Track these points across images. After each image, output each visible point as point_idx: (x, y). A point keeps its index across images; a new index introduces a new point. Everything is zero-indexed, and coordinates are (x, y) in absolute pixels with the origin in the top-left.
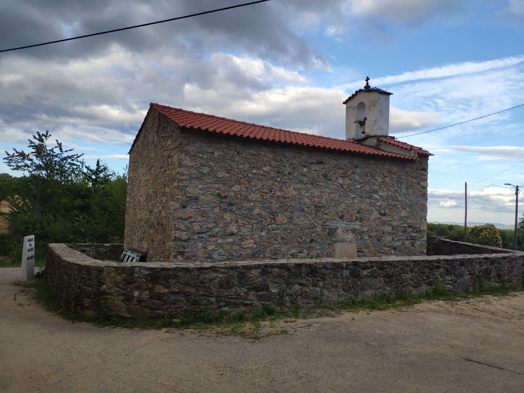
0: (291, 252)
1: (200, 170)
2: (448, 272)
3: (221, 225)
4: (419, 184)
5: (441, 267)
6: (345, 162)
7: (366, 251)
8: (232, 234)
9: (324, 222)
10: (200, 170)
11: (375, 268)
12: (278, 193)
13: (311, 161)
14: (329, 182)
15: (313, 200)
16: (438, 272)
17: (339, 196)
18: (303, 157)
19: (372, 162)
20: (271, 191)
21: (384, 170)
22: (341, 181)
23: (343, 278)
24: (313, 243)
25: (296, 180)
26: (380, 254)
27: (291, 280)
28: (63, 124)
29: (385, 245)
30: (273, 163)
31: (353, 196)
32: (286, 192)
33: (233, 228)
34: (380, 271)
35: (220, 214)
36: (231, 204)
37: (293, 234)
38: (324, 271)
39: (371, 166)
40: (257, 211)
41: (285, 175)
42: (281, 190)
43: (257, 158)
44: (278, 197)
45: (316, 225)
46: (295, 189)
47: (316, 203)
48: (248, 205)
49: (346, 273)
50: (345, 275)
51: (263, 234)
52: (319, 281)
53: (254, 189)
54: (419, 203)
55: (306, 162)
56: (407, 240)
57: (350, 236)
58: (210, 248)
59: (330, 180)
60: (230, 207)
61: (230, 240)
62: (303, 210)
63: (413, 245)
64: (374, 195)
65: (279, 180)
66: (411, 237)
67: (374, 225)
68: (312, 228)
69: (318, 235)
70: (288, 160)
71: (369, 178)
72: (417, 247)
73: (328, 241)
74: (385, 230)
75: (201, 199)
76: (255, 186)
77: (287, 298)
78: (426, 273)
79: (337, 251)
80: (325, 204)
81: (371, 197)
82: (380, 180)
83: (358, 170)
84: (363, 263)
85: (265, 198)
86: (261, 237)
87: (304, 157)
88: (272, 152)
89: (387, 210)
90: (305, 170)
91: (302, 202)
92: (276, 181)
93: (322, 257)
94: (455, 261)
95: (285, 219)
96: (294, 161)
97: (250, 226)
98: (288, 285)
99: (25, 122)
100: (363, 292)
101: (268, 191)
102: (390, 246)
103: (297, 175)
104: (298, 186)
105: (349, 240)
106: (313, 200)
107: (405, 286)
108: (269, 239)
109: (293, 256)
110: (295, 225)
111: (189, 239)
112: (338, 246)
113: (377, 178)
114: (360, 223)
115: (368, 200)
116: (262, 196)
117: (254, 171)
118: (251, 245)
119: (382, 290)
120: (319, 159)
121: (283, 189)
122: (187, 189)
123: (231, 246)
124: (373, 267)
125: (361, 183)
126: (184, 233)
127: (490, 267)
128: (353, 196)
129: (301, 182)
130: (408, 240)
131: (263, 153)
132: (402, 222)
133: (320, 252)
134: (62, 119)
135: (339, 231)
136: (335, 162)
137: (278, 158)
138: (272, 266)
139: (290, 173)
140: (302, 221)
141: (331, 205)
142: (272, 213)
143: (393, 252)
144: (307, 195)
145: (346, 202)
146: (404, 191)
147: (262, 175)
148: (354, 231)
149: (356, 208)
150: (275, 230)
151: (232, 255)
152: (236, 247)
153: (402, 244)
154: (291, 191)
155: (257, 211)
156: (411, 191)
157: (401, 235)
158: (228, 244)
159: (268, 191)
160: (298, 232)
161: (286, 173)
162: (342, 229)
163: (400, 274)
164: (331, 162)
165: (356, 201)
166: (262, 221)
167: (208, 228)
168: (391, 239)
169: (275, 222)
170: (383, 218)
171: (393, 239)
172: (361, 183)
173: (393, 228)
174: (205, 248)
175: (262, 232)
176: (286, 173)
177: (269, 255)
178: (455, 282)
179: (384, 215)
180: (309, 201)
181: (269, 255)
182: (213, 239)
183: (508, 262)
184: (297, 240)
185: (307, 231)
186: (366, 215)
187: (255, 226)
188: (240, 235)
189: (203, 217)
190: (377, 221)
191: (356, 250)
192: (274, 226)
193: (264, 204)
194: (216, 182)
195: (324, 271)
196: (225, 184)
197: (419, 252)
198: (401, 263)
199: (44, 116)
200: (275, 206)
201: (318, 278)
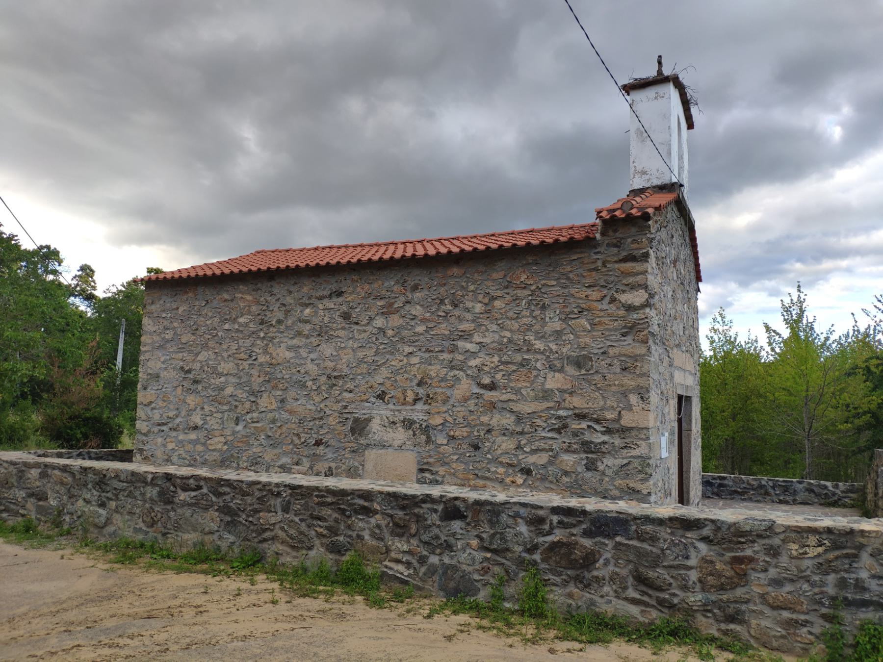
0: (280, 463)
1: (163, 336)
2: (400, 529)
3: (183, 413)
4: (613, 300)
5: (376, 512)
6: (389, 283)
7: (442, 470)
8: (196, 428)
9: (346, 407)
10: (163, 336)
11: (205, 490)
12: (262, 359)
13: (320, 293)
14: (356, 327)
15: (322, 366)
16: (368, 522)
17: (377, 353)
18: (305, 288)
19: (455, 271)
20: (250, 356)
21: (490, 283)
22: (379, 322)
23: (145, 501)
24: (322, 447)
25: (290, 332)
26: (481, 482)
27: (74, 492)
28: (829, 271)
29: (495, 461)
30: (254, 308)
31: (408, 349)
32: (274, 355)
33: (197, 419)
34: (214, 499)
35: (182, 397)
36: (196, 382)
37: (284, 429)
38: (116, 484)
39: (452, 282)
40: (229, 390)
41: (271, 325)
42: (266, 352)
43: (231, 305)
44: (261, 365)
45: (328, 412)
46: (289, 348)
47: (329, 372)
48: (218, 381)
49: (152, 492)
50: (149, 495)
51: (239, 428)
52: (110, 499)
53: (225, 355)
54: (611, 352)
55: (309, 298)
56: (567, 451)
57: (400, 435)
58: (171, 446)
59: (357, 324)
60: (195, 387)
61: (193, 436)
62: (304, 386)
63: (591, 466)
64: (461, 344)
65: (262, 335)
66: (585, 444)
67: (461, 412)
68: (321, 419)
69: (331, 431)
70: (278, 300)
71: (449, 307)
72: (609, 472)
73: (351, 445)
74: (494, 422)
75: (162, 376)
76: (227, 351)
77: (67, 518)
78: (325, 520)
79: (369, 466)
80: (346, 370)
81: (453, 350)
82: (479, 308)
83: (418, 295)
84: (178, 477)
85: (241, 368)
86: (234, 433)
87: (305, 289)
88: (254, 290)
89: (499, 376)
90: (307, 311)
91: (303, 371)
92: (259, 337)
93: (337, 475)
94: (424, 501)
95: (274, 402)
96: (289, 300)
97: (220, 415)
98: (70, 498)
99: (770, 280)
100: (180, 534)
101: (246, 357)
102: (510, 465)
103: (293, 323)
104: (295, 342)
105: (397, 443)
106: (322, 366)
107: (265, 540)
108: (247, 437)
109: (284, 469)
110: (291, 412)
111: (149, 431)
112: (372, 455)
113: (469, 305)
114: (426, 407)
115: (446, 356)
116: (237, 365)
117: (227, 326)
118: (219, 446)
119: (215, 537)
120: (334, 287)
121: (270, 350)
122: (149, 364)
123: (195, 446)
124: (199, 488)
125: (428, 321)
126: (146, 423)
127: (587, 542)
128: (408, 349)
129: (299, 334)
130: (574, 452)
131: (240, 295)
132: (551, 404)
133: (333, 465)
134: (827, 264)
135: (375, 425)
136: (367, 287)
137: (262, 299)
138: (54, 467)
139: (279, 322)
140: (303, 406)
141: (359, 371)
142: (253, 393)
143: (520, 481)
144: (312, 356)
145: (393, 363)
146: (557, 325)
147: (238, 331)
148: (408, 424)
149: (415, 376)
150: (258, 422)
151: (195, 460)
152: (200, 448)
153: (550, 463)
154: (283, 353)
155: (229, 390)
156: (584, 322)
157: (545, 438)
158: (190, 442)
159: (246, 357)
160: (293, 426)
161: (274, 322)
162: (382, 419)
163: (256, 511)
164: (359, 289)
165: (414, 360)
166: (236, 407)
167: (168, 417)
168: (512, 446)
169: (257, 408)
170: (488, 395)
171: (519, 447)
172: (428, 321)
173: (519, 419)
174: (164, 446)
175: (237, 424)
176: (274, 322)
177: (245, 464)
178: (422, 560)
179: (492, 387)
180: (316, 368)
181: (245, 464)
182: (174, 434)
183: (705, 539)
184: (292, 441)
185: (311, 424)
186: (439, 390)
187: (226, 416)
188: (206, 429)
189: (165, 401)
190: (472, 403)
191: (414, 468)
192: (255, 415)
193: (240, 378)
194: (181, 350)
195: (116, 484)
196: (190, 352)
197: (621, 490)
198: (259, 486)
199: (798, 266)
200: (257, 381)
201: (109, 495)
